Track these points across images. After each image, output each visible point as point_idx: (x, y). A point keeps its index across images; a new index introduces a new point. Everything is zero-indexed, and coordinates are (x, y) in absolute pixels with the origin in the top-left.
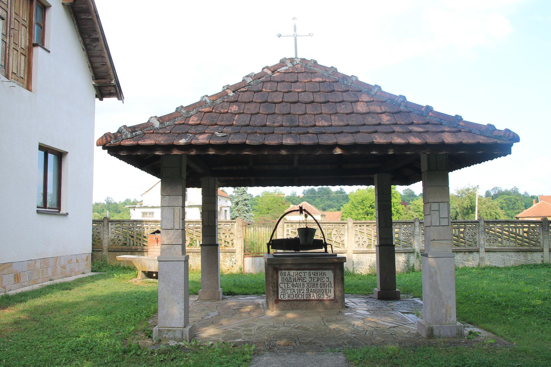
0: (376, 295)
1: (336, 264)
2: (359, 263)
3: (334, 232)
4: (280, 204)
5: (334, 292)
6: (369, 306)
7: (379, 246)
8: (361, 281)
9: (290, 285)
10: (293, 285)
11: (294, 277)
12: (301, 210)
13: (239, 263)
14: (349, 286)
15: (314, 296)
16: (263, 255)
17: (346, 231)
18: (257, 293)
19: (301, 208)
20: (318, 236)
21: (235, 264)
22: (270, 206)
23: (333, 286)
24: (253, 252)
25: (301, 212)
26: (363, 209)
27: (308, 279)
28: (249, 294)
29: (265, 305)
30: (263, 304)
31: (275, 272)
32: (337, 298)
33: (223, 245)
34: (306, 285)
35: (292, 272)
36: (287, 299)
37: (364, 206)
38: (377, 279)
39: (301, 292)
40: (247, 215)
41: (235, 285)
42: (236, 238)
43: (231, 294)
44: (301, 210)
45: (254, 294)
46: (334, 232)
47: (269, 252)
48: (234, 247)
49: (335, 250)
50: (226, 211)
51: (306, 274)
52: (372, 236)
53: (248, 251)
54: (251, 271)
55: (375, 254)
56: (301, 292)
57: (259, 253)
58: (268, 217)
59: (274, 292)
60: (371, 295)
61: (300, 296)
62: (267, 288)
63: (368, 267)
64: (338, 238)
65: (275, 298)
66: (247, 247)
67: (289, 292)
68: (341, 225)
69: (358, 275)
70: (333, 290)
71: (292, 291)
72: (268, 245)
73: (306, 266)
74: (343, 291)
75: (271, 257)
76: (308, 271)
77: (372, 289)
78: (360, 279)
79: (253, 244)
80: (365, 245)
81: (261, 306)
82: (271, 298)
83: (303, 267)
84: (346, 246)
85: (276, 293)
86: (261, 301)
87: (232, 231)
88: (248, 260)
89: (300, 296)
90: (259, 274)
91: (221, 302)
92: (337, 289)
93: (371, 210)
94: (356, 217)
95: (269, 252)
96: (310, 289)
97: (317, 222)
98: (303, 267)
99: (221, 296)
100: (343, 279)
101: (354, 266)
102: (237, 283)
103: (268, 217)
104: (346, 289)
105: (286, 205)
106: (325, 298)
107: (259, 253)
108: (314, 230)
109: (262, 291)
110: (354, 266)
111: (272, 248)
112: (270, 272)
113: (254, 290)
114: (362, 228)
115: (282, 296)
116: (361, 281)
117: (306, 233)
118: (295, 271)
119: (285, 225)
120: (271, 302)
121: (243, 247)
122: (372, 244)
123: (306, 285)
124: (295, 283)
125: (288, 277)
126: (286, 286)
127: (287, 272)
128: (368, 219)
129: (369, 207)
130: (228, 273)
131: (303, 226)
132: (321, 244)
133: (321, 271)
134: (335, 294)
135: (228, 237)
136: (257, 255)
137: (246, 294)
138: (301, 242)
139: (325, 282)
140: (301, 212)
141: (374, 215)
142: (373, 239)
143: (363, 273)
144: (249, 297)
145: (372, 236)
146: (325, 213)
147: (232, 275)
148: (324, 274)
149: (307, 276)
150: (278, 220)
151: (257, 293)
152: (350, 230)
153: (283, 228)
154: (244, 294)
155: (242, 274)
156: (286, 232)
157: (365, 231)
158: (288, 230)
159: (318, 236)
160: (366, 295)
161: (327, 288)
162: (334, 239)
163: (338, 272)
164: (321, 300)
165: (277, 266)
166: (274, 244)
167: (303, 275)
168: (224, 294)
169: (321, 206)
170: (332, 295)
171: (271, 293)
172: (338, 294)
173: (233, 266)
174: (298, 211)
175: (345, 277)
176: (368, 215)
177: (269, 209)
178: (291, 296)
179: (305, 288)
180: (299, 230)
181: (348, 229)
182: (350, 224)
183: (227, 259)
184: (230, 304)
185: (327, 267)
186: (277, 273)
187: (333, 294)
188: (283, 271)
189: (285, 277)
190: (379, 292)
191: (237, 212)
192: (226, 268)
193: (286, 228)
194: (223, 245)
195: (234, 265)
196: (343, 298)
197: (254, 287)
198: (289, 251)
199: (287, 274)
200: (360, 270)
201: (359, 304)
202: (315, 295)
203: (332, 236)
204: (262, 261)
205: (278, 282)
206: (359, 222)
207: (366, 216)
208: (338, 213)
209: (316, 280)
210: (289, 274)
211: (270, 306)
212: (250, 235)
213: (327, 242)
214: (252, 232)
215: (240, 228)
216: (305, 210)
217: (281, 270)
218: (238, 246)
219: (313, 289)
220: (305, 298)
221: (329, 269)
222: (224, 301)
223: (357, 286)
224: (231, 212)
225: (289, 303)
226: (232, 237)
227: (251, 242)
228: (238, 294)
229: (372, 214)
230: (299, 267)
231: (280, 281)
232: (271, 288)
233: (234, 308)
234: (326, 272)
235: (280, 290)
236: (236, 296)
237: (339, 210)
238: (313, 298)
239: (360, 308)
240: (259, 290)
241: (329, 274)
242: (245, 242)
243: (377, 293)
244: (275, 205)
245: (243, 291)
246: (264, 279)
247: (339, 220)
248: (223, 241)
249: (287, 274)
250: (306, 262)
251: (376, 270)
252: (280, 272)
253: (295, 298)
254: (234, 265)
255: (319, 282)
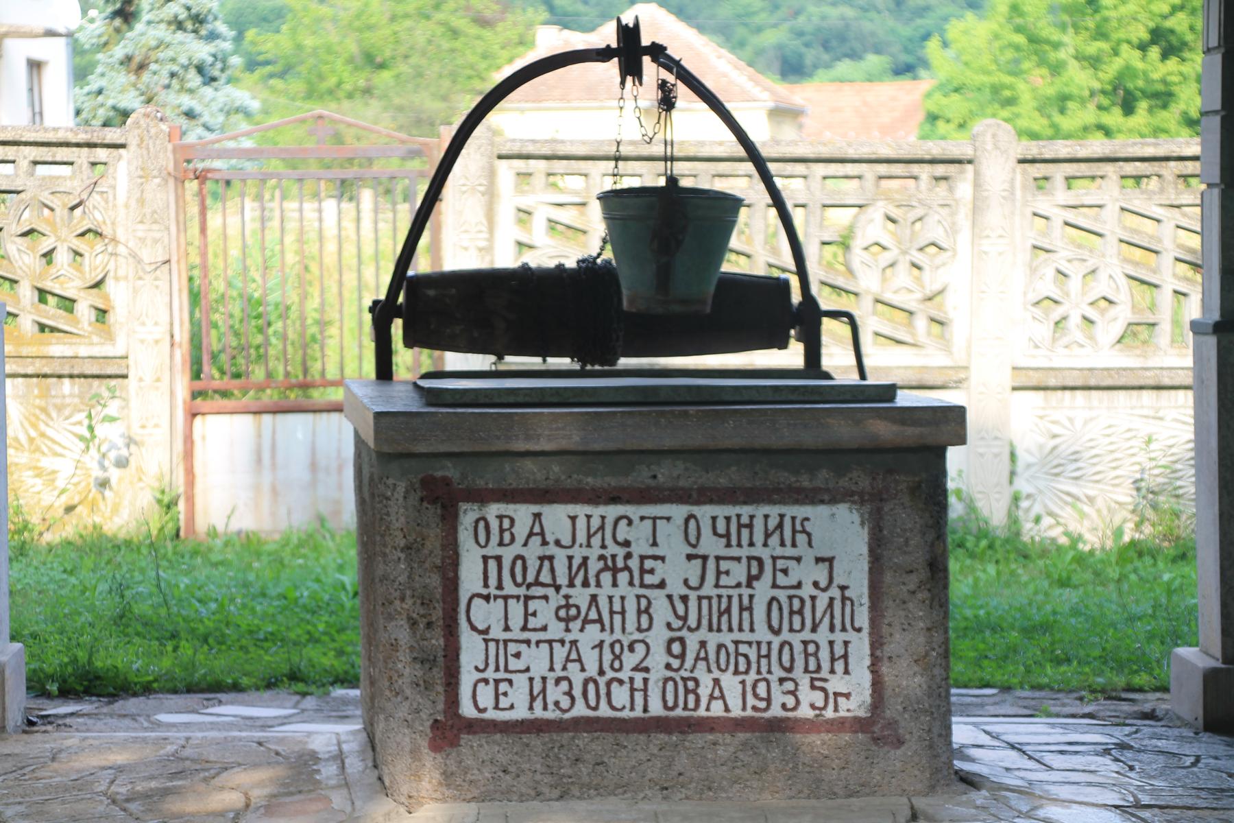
0: (1187, 700)
1: (895, 459)
2: (1060, 463)
3: (873, 228)
4: (461, 23)
5: (874, 669)
6: (1134, 780)
7: (1218, 328)
8: (1070, 597)
9: (545, 613)
10: (567, 613)
11: (578, 553)
12: (630, 52)
13: (157, 459)
14: (978, 627)
15: (729, 696)
16: (337, 395)
17: (963, 217)
18: (293, 680)
19: (629, 34)
20: (754, 249)
21: (122, 463)
22: (380, 39)
23: (863, 619)
24: (259, 374)
25: (631, 69)
26: (1094, 62)
27: (676, 571)
28: (236, 688)
29: (355, 765)
30: (340, 758)
31: (432, 513)
32: (893, 710)
33: (26, 323)
34: (662, 611)
35: (557, 517)
36: (521, 713)
37: (1100, 34)
38: (1202, 584)
39: (630, 660)
40: (210, 101)
41: (122, 619)
42: (124, 267)
43: (91, 685)
44: (630, 52)
45: (271, 684)
46: (873, 228)
47: (384, 370)
48: (110, 337)
49: (885, 363)
50: (35, 66)
51: (667, 536)
52: (1167, 259)
53: (230, 365)
54: (245, 521)
55: (1186, 399)
56: (630, 660)
57: (305, 386)
58: (369, 122)
59: (425, 660)
60: (1150, 701)
61: (620, 695)
62: (371, 640)
63: (1125, 495)
64: (903, 277)
65: (433, 708)
66: (213, 341)
67: (537, 660)
68: (924, 171)
69: (1048, 550)
70: (861, 647)
71: (560, 652)
72: (382, 313)
73: (666, 473)
74: (939, 660)
75: (401, 399)
76: (679, 512)
77: (1155, 650)
78: (1064, 583)
79: (257, 313)
80: (1111, 326)
81: (328, 771)
82: (403, 711)
83: (641, 476)
84: (958, 332)
85: (438, 674)
86: (328, 733)
87: (96, 214)
88: (226, 436)
89: (620, 695)
90: (309, 542)
91: (17, 745)
92: (897, 642)
93: (1157, 68)
94: (1039, 124)
95: (384, 370)
96: (692, 641)
97: (753, 154)
98: (641, 476)
99: (17, 700)
100: (937, 571)
101: (1022, 485)
102: (142, 608)
103: (369, 122)
104: (963, 647)
105: (507, 29)
106: (805, 712)
107: (305, 386)
108: (727, 206)
109: (328, 660)
110: (1022, 485)
111: (409, 342)
112: (398, 515)
113: (274, 659)
114: (1086, 193)
115: (486, 696)
116: (1070, 597)
117: (669, 222)
118: (581, 510)
119: (506, 169)
120: (406, 739)
121: (182, 335)
122: (1164, 316)
123: (662, 611)
124: (580, 597)
125: (533, 552)
126: (516, 620)
127: (523, 514)
128: (1134, 133)
129: (1143, 47)
130: (69, 530)
131: (650, 177)
132: (775, 310)
133: (774, 511)
134: (877, 684)
135: (62, 257)
136: (297, 397)
137: (214, 688)
138: (632, 292)
139: (807, 591)
140: (631, 69)
141: (1176, 109)
142: (1170, 285)
143: (1092, 540)
144: (231, 709)
145: (1167, 259)
146: (800, 94)
147: (98, 549)
148: (801, 529)
149: (672, 543)
150: (447, 134)
151: (294, 676)
152: (994, 216)
153: (491, 194)
154: (190, 690)
155: (173, 542)
156: (525, 214)
157: (1109, 221)
158: (525, 214)
159: (754, 249)
160: (1109, 694)
161: (823, 636)
162: (868, 281)
163: (905, 518)
164: (777, 727)
165: (450, 471)
166: (425, 306)
167: (639, 536)
168: (37, 687)
169: (770, 38)
170: (854, 690)
171: (407, 670)
172: (907, 679)
173: (104, 484)
174: (603, 55)
175: (953, 566)
176: (1128, 108)
177: (372, 61)
178: (554, 693)
179: (658, 637)
180: (613, 201)
181: (977, 208)
182: (999, 169)
183: (65, 431)
184: (92, 761)
185: (823, 477)
186: (450, 520)
187: (867, 678)
188: (493, 510)
189: (508, 554)
190: (1210, 677)
191: (123, 78)
192: (48, 498)
193: (509, 198)
194: (26, 323)
195: (114, 474)
196: (939, 715)
197: (271, 637)
198: (534, 362)
199: (521, 531)
200: (1067, 514)
201: (1057, 761)
202: (730, 682)
203: (858, 256)
204: (335, 440)
205: (452, 585)
206: (1062, 148)
207: (1114, 118)
208: (906, 95)
209: (739, 572)
210: (538, 532)
211: (398, 769)
212: (234, 252)
213: (826, 301)
214: (252, 226)
215: (161, 195)
216: (657, 52)
217: (482, 497)
218: (148, 329)
219: (713, 640)
220: (656, 709)
221: (834, 498)
222: (41, 743)
223: (1045, 627)
224: (80, 74)
225: (536, 741)
226: (96, 259)
227: (248, 300)
228: (147, 690)
229: (1163, 97)
230: (610, 476)
231: (470, 578)
232: (403, 634)
233: (122, 789)
234: (818, 516)
235: (471, 651)
236: (132, 705)
237: (905, 70)
238: (717, 709)
239: (1065, 792)
240: (312, 652)
241: (841, 530)
242: (195, 297)
243: (1196, 687)
244: (422, 32)
245: (191, 666)
246: (350, 578)
247: (910, 142)
248: (26, 292)
249: (521, 531)
250: (668, 443)
251: (1194, 510)
252: (468, 515)
253: (580, 710)
254: (114, 474)
255: (763, 590)
